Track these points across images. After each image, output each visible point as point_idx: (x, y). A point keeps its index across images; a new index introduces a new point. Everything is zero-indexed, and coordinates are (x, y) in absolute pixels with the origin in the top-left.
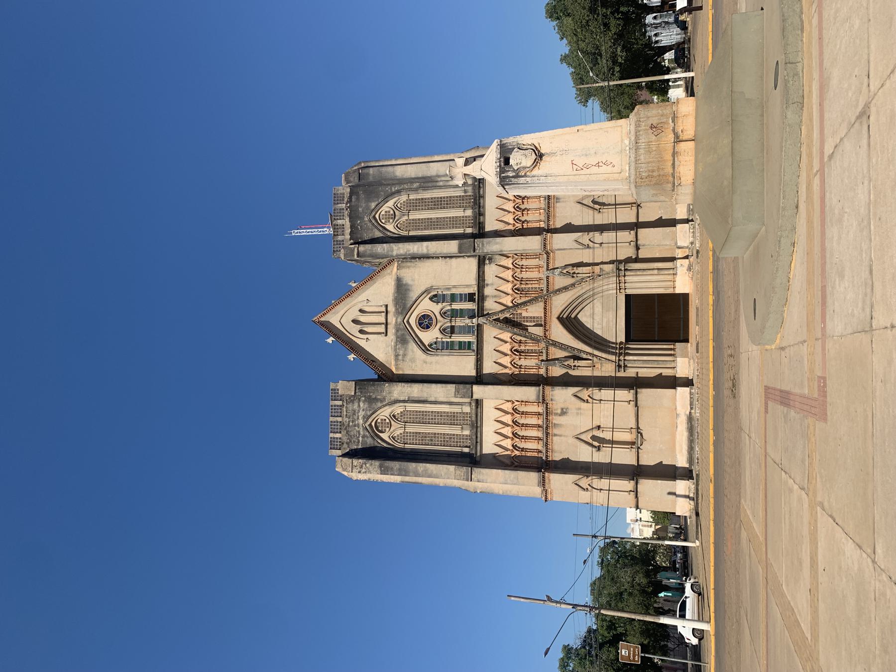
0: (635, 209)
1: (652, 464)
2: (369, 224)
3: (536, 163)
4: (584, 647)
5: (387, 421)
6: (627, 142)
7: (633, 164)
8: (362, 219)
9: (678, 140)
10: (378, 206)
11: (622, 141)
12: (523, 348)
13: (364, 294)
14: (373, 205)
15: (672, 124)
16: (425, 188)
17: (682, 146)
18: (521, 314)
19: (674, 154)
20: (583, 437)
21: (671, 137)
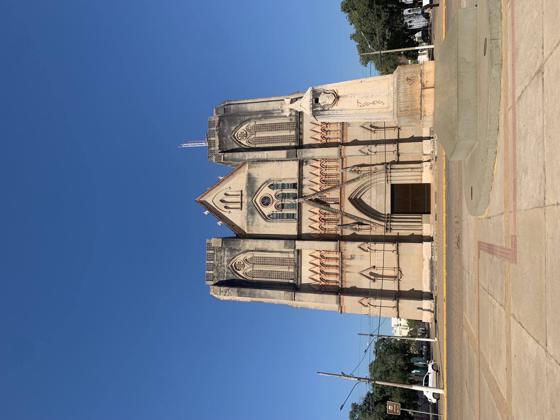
0: (397, 130)
1: (408, 290)
2: (231, 140)
3: (335, 102)
4: (365, 405)
5: (242, 263)
6: (392, 89)
7: (396, 103)
8: (226, 137)
9: (424, 87)
10: (237, 129)
11: (389, 88)
12: (327, 217)
13: (227, 184)
14: (233, 128)
15: (420, 78)
16: (266, 118)
17: (426, 91)
18: (325, 196)
19: (421, 96)
20: (364, 273)
21: (419, 86)
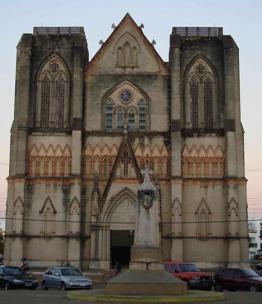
0: (138, 241)
1: (242, 120)
2: (195, 54)
3: (144, 206)
4: (51, 67)
5: (57, 69)
6: (150, 244)
7: (140, 246)
8: (199, 49)
9: (148, 264)
10: (208, 61)
11: (150, 242)
12: (107, 164)
13: (146, 51)
14: (209, 57)
15: (154, 262)
16: (218, 96)
17: (145, 266)
18: (130, 163)
19: (142, 262)
20: (48, 203)
21: (149, 261)
